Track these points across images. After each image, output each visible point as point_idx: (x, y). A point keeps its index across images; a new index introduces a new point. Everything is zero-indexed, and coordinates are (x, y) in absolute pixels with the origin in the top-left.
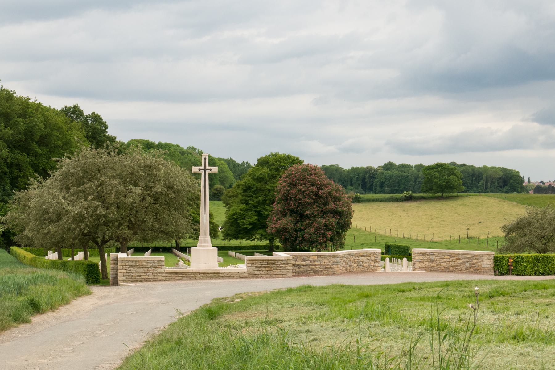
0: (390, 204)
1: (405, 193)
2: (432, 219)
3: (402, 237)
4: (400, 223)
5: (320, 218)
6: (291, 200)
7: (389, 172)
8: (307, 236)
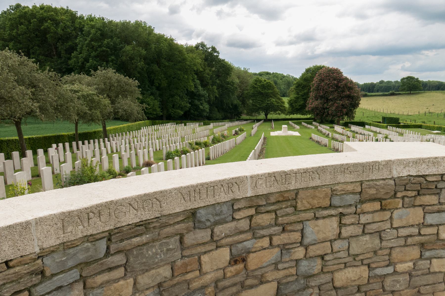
0: (382, 97)
1: (391, 92)
3: (390, 113)
6: (321, 90)
8: (330, 112)
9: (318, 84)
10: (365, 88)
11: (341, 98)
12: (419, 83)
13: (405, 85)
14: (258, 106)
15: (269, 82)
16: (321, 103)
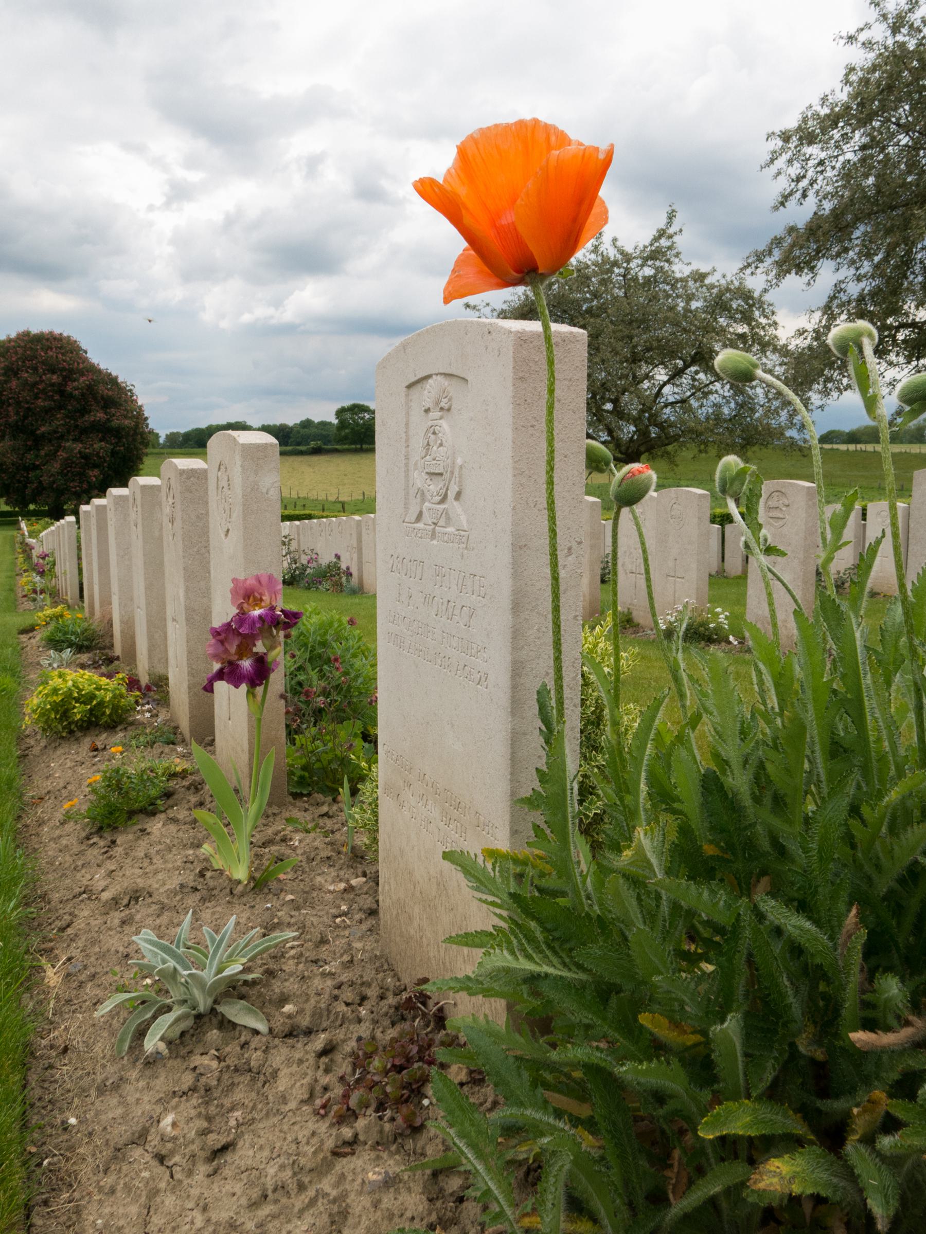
2: (345, 475)
8: (45, 479)
11: (81, 433)
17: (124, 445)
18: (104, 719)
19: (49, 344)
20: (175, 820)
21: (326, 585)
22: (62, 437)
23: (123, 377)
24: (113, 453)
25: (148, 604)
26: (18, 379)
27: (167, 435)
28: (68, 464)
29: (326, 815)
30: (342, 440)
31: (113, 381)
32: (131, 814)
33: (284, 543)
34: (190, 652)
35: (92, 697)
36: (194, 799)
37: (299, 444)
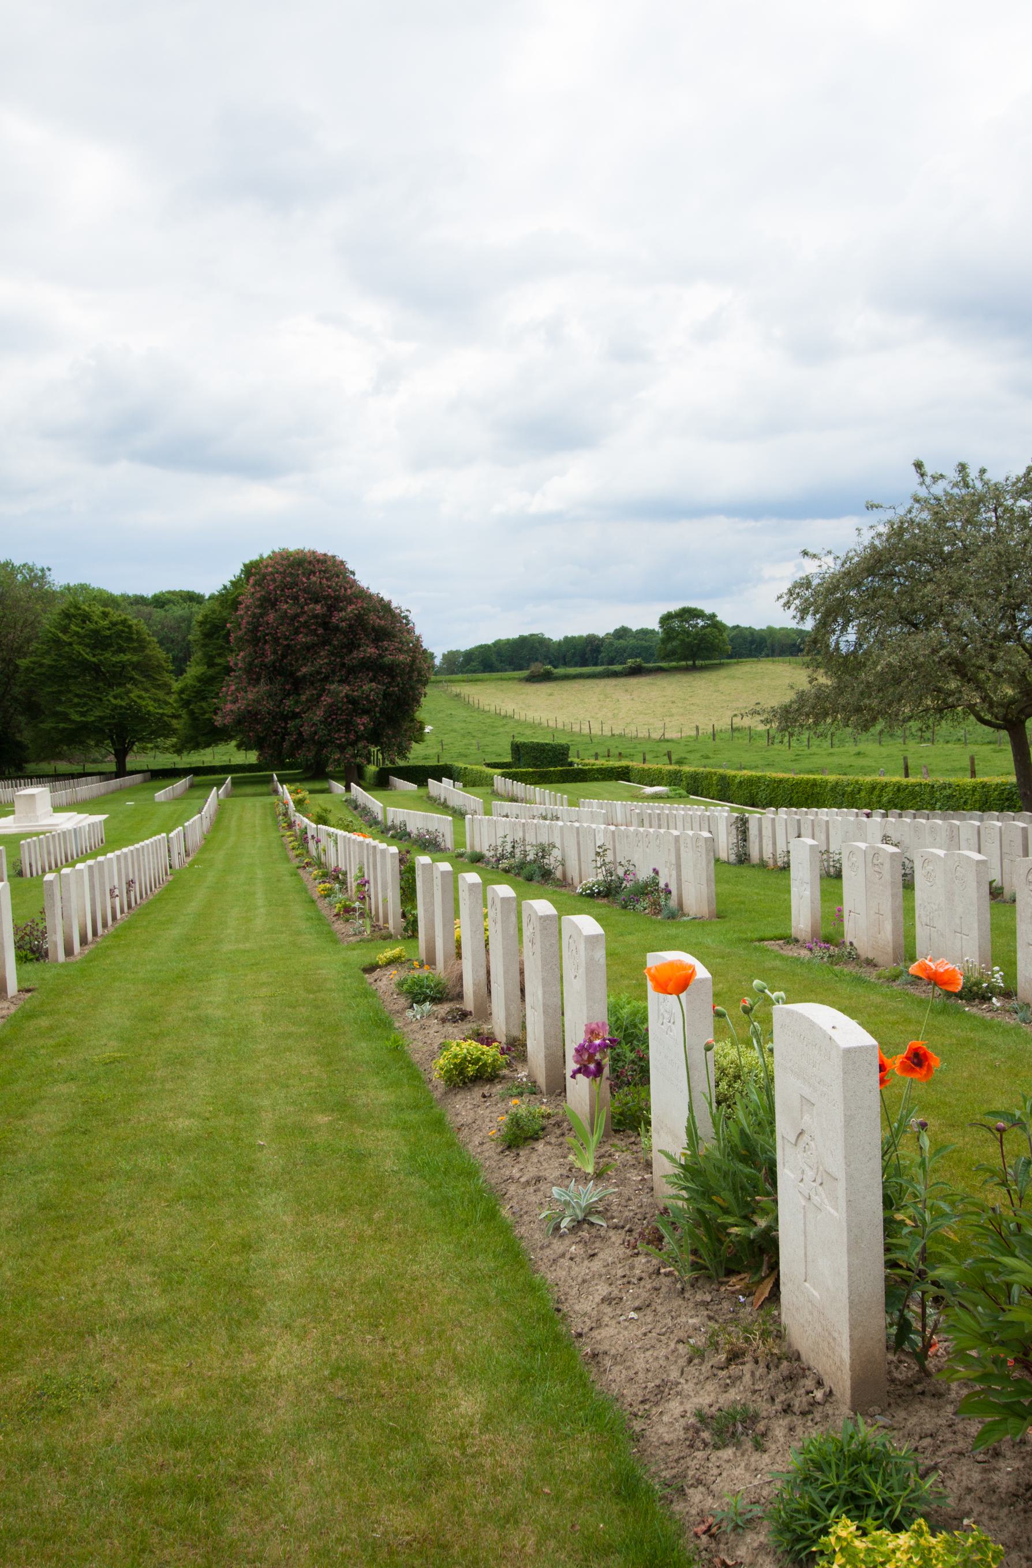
1: (630, 662)
2: (673, 702)
4: (616, 711)
5: (339, 681)
7: (621, 641)
8: (306, 730)
9: (254, 615)
10: (569, 654)
11: (349, 673)
12: (720, 630)
13: (674, 638)
14: (76, 717)
15: (124, 622)
16: (270, 695)
17: (398, 686)
18: (487, 1075)
19: (311, 567)
20: (549, 1143)
21: (645, 903)
22: (326, 679)
23: (398, 601)
24: (386, 696)
25: (506, 984)
26: (276, 611)
27: (444, 655)
28: (332, 711)
29: (633, 1143)
30: (668, 656)
31: (385, 608)
32: (526, 1139)
33: (598, 854)
34: (546, 1034)
35: (479, 1059)
36: (558, 1132)
37: (611, 662)
